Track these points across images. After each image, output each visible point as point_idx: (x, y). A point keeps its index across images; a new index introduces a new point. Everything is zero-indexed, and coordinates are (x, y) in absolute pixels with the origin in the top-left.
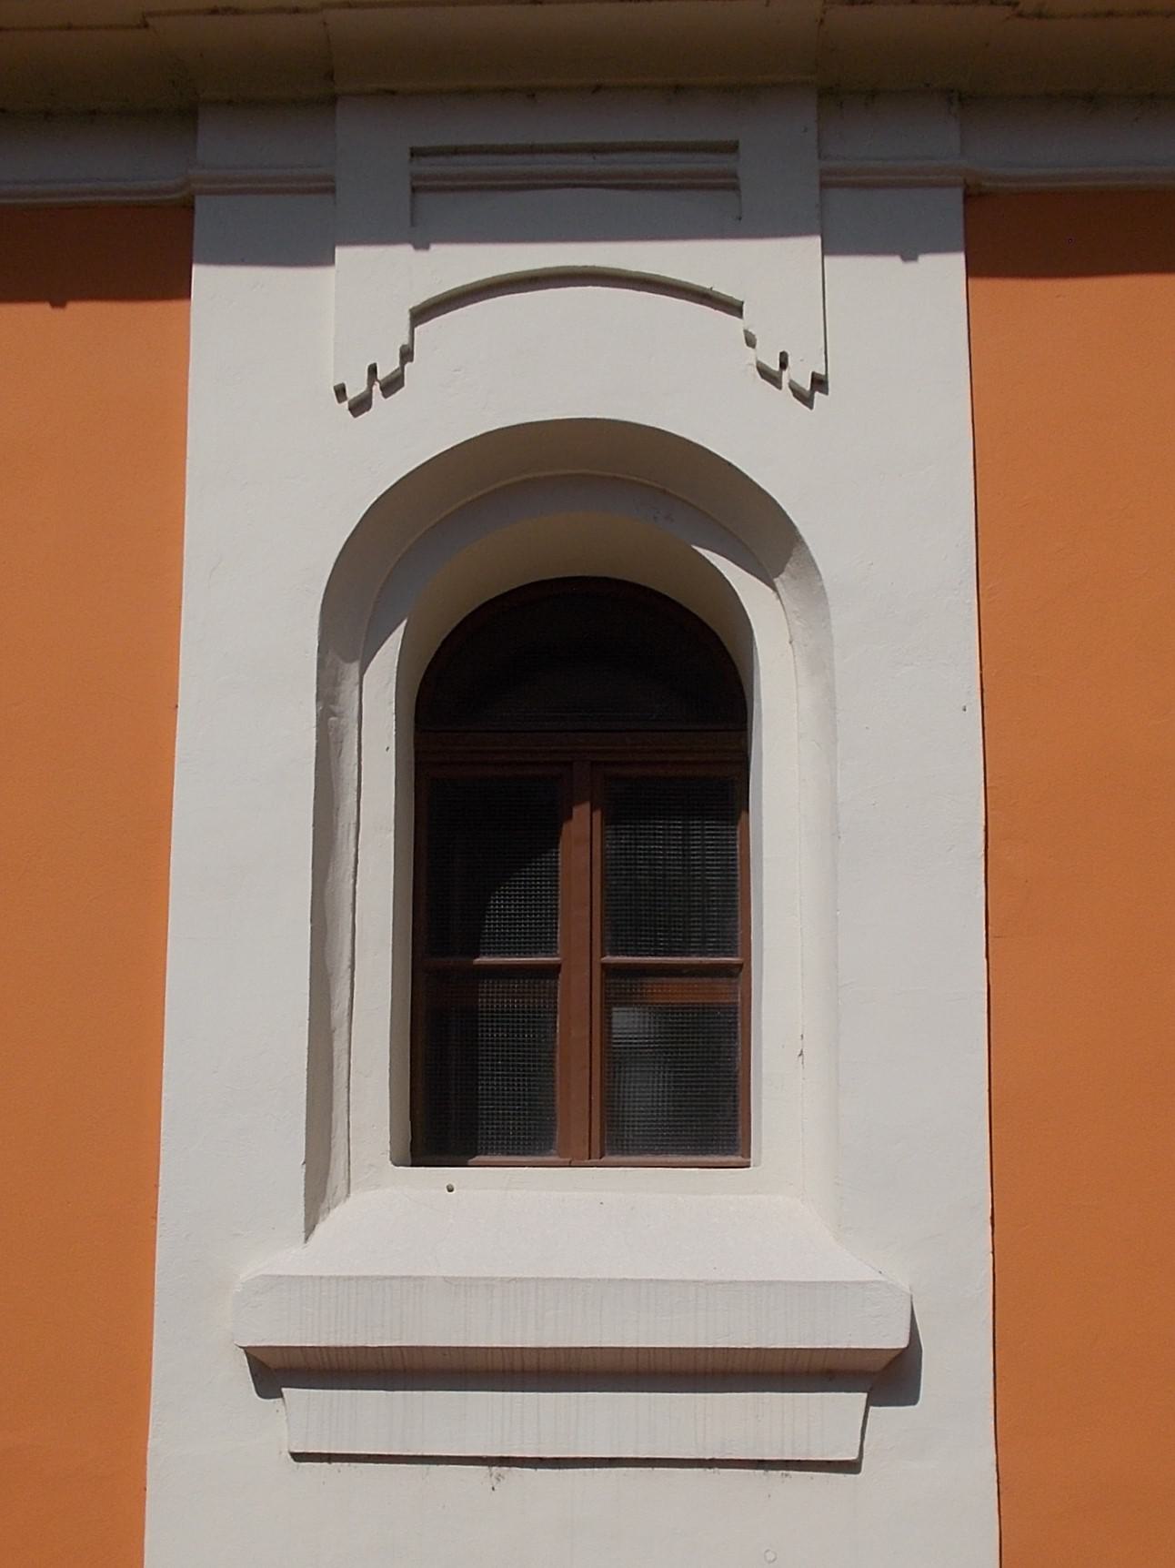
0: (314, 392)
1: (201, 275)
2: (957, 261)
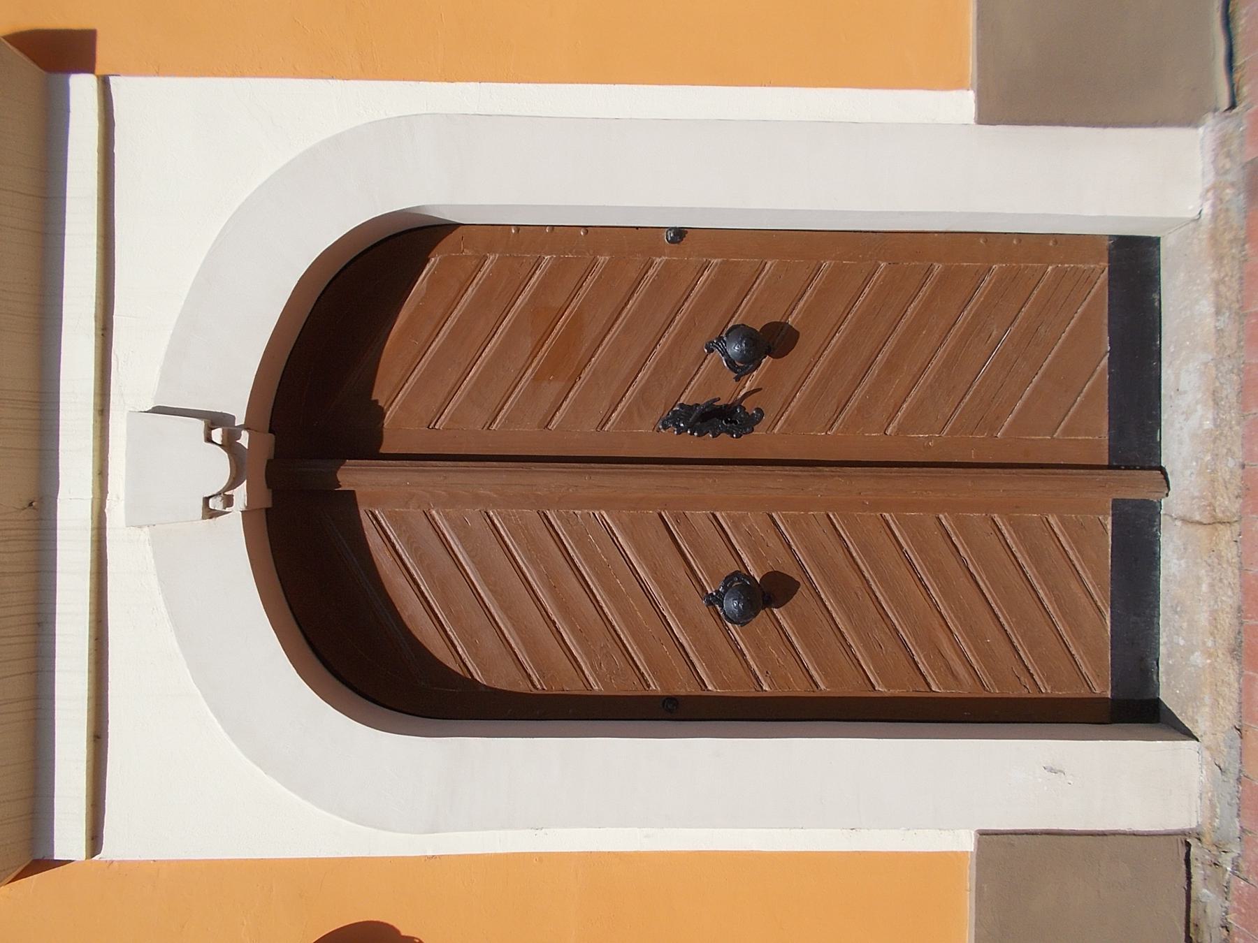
2: (964, 103)
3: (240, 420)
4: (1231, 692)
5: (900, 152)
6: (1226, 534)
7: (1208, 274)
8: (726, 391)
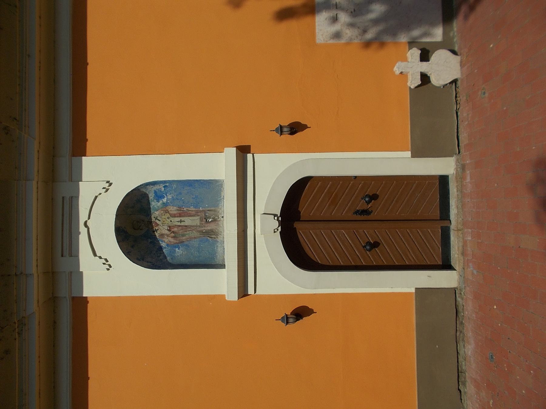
0: (106, 272)
1: (84, 296)
2: (408, 154)
3: (279, 215)
4: (462, 262)
5: (397, 162)
6: (460, 232)
7: (455, 185)
8: (365, 207)
